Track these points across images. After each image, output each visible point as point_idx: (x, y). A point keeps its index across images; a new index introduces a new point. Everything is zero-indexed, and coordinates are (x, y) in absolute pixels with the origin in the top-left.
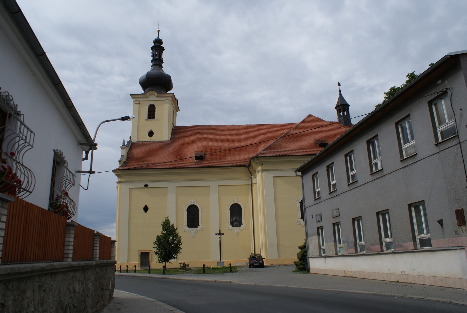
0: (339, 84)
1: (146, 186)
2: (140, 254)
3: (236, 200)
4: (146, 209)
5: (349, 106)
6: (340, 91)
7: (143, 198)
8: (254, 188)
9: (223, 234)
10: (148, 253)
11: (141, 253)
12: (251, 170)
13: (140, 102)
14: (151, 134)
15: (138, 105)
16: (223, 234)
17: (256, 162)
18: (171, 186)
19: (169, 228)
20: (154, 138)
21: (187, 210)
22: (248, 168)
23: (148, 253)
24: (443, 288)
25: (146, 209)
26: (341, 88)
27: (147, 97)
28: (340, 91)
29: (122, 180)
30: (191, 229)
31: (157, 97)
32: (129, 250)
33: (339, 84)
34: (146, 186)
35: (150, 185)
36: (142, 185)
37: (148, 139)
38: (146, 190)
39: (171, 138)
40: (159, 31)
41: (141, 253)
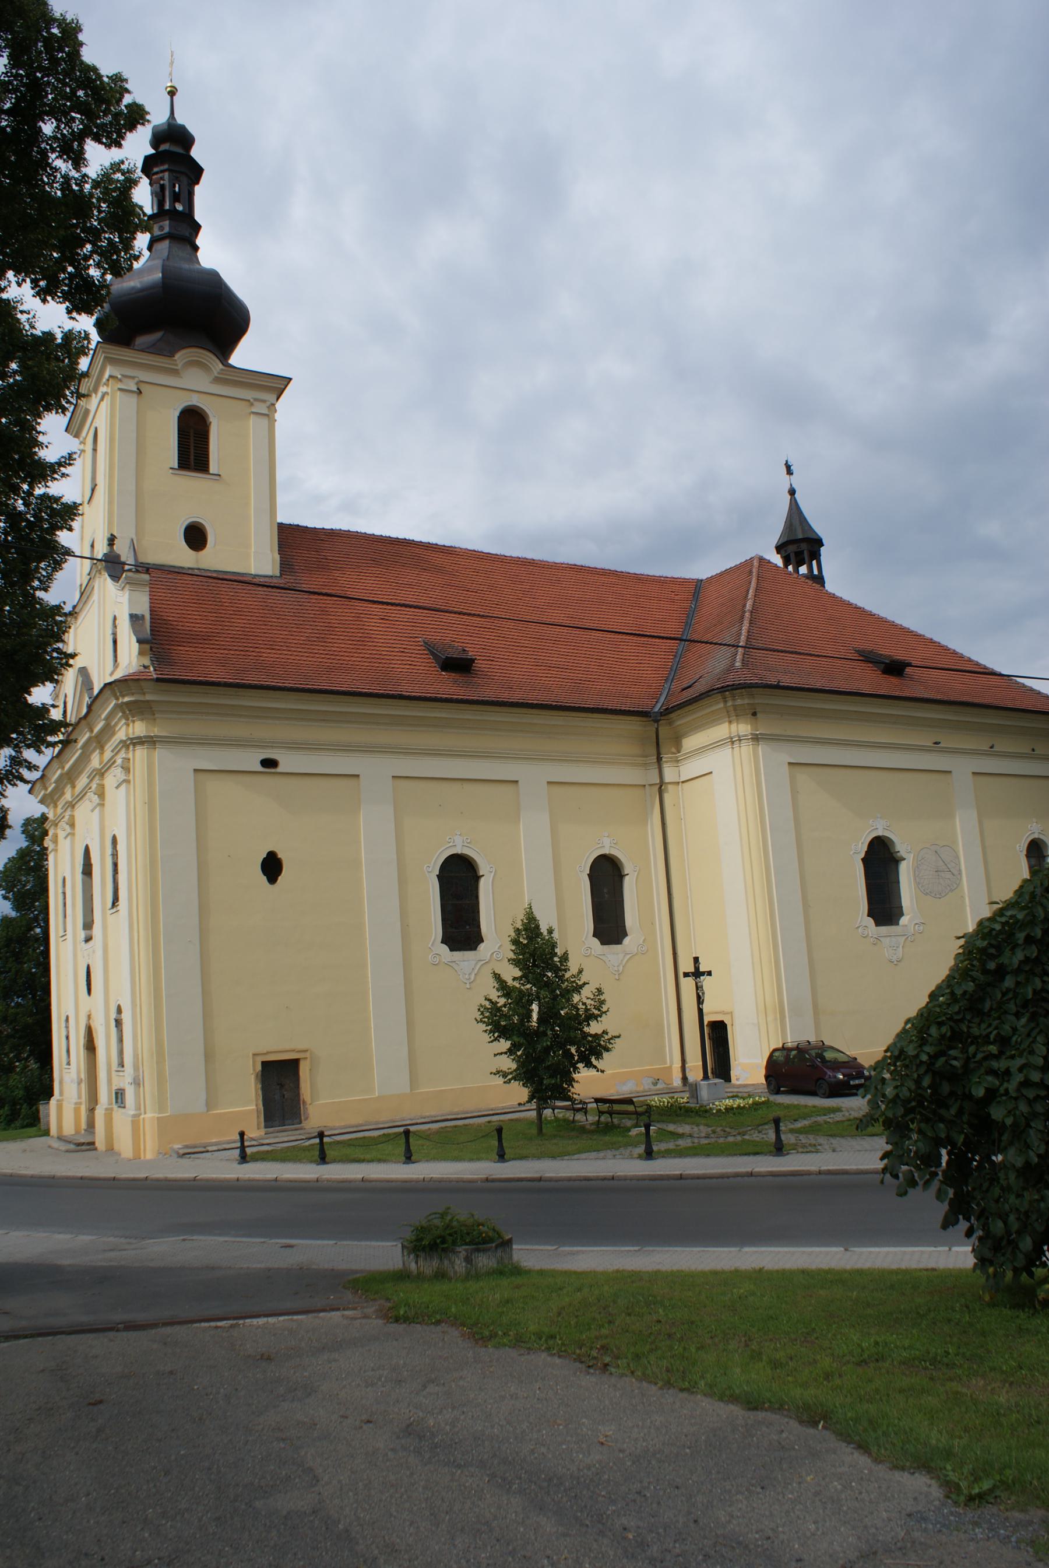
0: (789, 471)
1: (269, 763)
2: (259, 1068)
3: (607, 842)
4: (272, 867)
5: (823, 545)
6: (792, 492)
7: (256, 817)
8: (667, 797)
9: (709, 973)
10: (295, 1063)
11: (264, 1064)
12: (664, 731)
13: (143, 387)
14: (195, 536)
15: (133, 399)
16: (709, 973)
17: (739, 702)
18: (376, 771)
19: (535, 951)
20: (214, 558)
21: (440, 877)
22: (657, 724)
23: (295, 1063)
24: (11, 1175)
25: (272, 867)
26: (796, 481)
27: (175, 372)
28: (792, 492)
29: (156, 731)
30: (458, 955)
31: (217, 380)
32: (209, 1056)
33: (789, 471)
34: (269, 763)
35: (288, 762)
36: (252, 760)
37: (184, 557)
38: (269, 782)
39: (283, 564)
40: (172, 93)
41: (264, 1064)
